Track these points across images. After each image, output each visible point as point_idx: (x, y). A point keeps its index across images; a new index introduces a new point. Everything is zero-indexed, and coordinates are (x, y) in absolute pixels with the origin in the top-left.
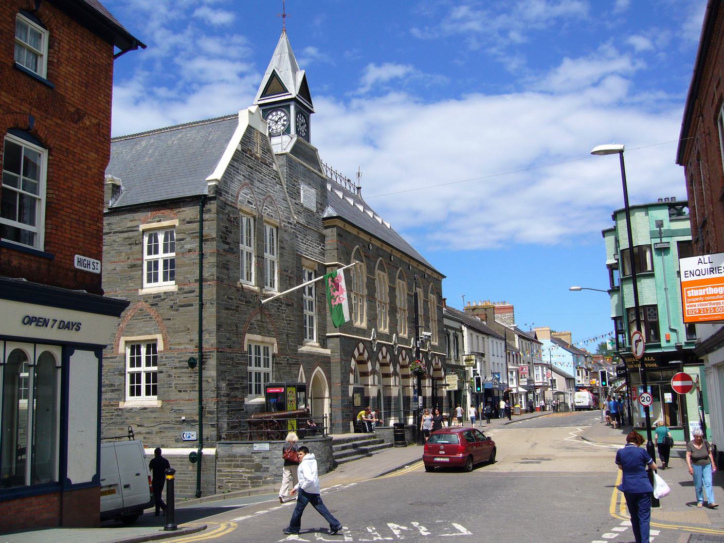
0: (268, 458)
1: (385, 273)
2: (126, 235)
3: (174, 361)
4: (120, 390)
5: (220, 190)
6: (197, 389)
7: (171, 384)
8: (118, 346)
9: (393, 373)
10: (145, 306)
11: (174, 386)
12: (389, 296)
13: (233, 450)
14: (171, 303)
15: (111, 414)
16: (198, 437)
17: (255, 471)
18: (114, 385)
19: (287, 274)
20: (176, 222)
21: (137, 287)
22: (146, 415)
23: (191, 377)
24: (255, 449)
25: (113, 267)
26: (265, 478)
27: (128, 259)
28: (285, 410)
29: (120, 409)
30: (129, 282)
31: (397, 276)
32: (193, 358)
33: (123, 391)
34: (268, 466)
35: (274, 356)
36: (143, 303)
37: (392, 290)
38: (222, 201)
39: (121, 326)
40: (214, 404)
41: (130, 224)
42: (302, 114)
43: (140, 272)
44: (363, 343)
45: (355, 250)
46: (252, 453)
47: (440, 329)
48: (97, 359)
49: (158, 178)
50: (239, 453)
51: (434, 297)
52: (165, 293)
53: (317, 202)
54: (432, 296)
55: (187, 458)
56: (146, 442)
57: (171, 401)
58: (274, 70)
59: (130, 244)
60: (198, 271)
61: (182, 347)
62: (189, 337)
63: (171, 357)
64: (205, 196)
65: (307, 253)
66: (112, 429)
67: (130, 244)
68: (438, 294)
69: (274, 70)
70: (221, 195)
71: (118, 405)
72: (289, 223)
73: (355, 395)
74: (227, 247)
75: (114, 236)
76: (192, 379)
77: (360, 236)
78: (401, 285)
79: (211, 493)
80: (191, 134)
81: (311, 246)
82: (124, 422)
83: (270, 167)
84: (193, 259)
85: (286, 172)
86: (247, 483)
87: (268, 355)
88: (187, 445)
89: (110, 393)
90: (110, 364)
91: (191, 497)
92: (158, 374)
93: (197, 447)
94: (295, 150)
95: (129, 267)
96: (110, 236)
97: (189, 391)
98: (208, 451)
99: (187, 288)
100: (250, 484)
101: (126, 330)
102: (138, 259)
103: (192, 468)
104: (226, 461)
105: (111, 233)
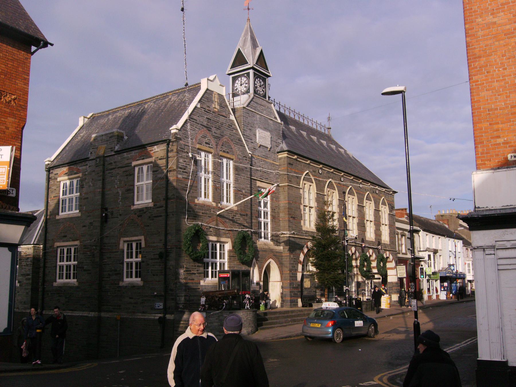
2: (124, 169)
4: (120, 274)
6: (163, 274)
23: (160, 265)
29: (120, 287)
36: (134, 215)
39: (121, 230)
48: (10, 253)
52: (146, 208)
59: (127, 175)
61: (155, 245)
67: (127, 175)
71: (119, 284)
75: (118, 170)
85: (243, 120)
98: (168, 316)
99: (158, 204)
102: (131, 185)
105: (116, 168)
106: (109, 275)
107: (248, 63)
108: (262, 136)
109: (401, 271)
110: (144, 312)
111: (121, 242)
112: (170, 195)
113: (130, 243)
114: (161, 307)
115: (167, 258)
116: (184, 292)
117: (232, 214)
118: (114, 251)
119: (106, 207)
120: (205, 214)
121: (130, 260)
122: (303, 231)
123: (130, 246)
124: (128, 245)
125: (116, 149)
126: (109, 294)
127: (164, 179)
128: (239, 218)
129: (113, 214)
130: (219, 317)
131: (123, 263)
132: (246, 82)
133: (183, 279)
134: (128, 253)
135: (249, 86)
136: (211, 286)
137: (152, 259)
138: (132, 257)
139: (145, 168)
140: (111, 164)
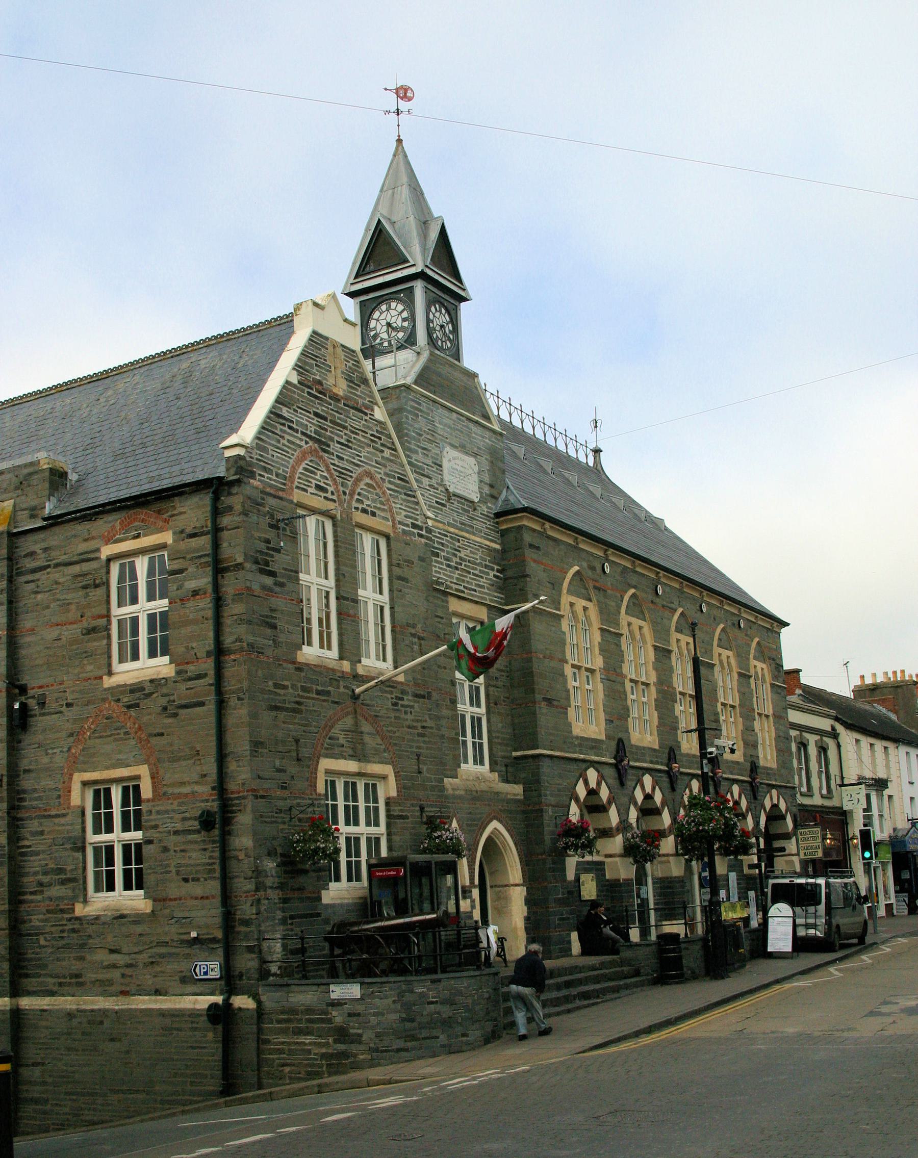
0: (359, 1015)
1: (645, 620)
2: (76, 569)
3: (171, 818)
4: (76, 882)
5: (250, 466)
6: (217, 874)
7: (168, 865)
8: (70, 792)
9: (670, 827)
10: (116, 709)
11: (173, 870)
12: (655, 669)
13: (291, 1000)
14: (163, 701)
15: (61, 928)
16: (223, 973)
17: (335, 1041)
18: (65, 870)
19: (413, 631)
20: (167, 537)
21: (99, 673)
22: (124, 929)
23: (205, 850)
24: (333, 996)
25: (55, 633)
26: (355, 1056)
27: (82, 616)
28: (407, 913)
29: (77, 919)
30: (85, 662)
31: (673, 628)
32: (208, 812)
33: (81, 882)
34: (360, 1031)
35: (388, 803)
36: (112, 703)
37: (663, 653)
38: (257, 488)
39: (74, 751)
40: (252, 905)
41: (83, 547)
42: (442, 305)
43: (105, 642)
44: (597, 770)
45: (570, 575)
46: (329, 1004)
47: (781, 734)
49: (137, 452)
50: (303, 1004)
51: (764, 666)
52: (152, 681)
53: (481, 481)
54: (760, 665)
55: (201, 1015)
56: (126, 985)
57: (171, 900)
58: (379, 220)
59: (85, 587)
60: (211, 634)
61: (186, 790)
62: (198, 768)
63: (167, 812)
64: (220, 479)
65: (462, 588)
66: (64, 959)
67: (85, 587)
68: (774, 660)
69: (379, 220)
70: (252, 475)
71: (73, 910)
72: (414, 526)
73: (583, 877)
74: (269, 581)
75: (56, 572)
76: (208, 854)
77: (581, 546)
78: (680, 643)
79: (251, 1088)
80: (205, 360)
81: (469, 573)
82: (85, 944)
83: (366, 414)
84: (202, 609)
86: (321, 1066)
87: (376, 800)
88: (202, 989)
89: (58, 887)
90: (57, 828)
91: (211, 1094)
92: (144, 847)
93: (221, 994)
94: (423, 378)
95: (84, 631)
96: (48, 573)
97: (202, 879)
98: (242, 1002)
99: (192, 669)
100: (324, 1068)
101: (81, 758)
102: (101, 617)
103: (211, 1037)
104: (279, 1022)
105: (49, 566)
106: (41, 884)
107: (408, 261)
108: (456, 467)
109: (810, 843)
110: (157, 992)
111: (76, 788)
112: (228, 640)
113: (102, 787)
114: (215, 974)
115: (227, 829)
116: (282, 927)
117: (391, 693)
118: (53, 813)
119: (24, 682)
120: (323, 695)
121: (104, 837)
122: (573, 737)
123: (102, 797)
124: (97, 793)
125: (47, 511)
126: (42, 942)
127: (205, 593)
128: (412, 704)
129: (44, 703)
130: (401, 995)
131: (83, 849)
132: (405, 315)
133: (276, 888)
134: (97, 817)
135: (414, 326)
136: (348, 904)
137: (176, 833)
138: (110, 830)
139: (142, 565)
140: (32, 554)
